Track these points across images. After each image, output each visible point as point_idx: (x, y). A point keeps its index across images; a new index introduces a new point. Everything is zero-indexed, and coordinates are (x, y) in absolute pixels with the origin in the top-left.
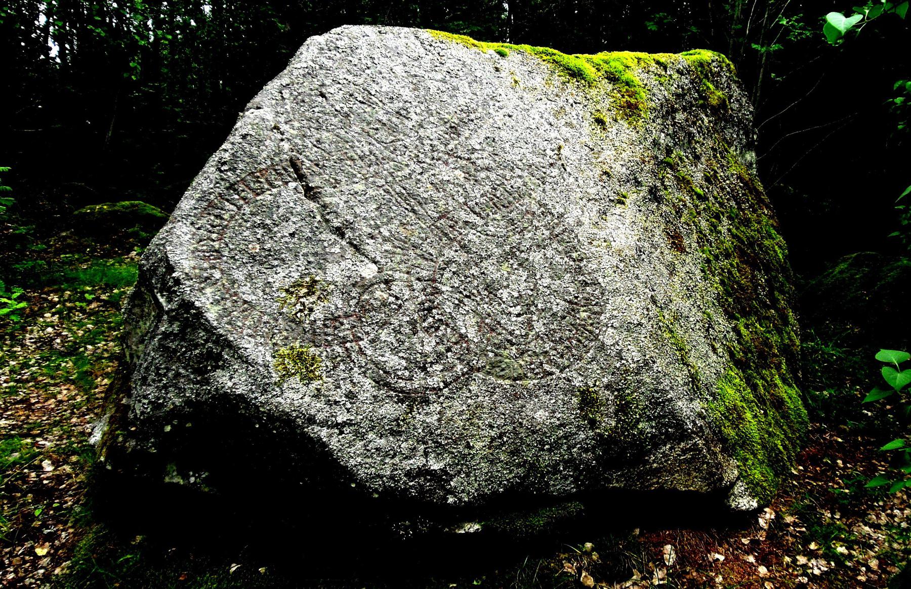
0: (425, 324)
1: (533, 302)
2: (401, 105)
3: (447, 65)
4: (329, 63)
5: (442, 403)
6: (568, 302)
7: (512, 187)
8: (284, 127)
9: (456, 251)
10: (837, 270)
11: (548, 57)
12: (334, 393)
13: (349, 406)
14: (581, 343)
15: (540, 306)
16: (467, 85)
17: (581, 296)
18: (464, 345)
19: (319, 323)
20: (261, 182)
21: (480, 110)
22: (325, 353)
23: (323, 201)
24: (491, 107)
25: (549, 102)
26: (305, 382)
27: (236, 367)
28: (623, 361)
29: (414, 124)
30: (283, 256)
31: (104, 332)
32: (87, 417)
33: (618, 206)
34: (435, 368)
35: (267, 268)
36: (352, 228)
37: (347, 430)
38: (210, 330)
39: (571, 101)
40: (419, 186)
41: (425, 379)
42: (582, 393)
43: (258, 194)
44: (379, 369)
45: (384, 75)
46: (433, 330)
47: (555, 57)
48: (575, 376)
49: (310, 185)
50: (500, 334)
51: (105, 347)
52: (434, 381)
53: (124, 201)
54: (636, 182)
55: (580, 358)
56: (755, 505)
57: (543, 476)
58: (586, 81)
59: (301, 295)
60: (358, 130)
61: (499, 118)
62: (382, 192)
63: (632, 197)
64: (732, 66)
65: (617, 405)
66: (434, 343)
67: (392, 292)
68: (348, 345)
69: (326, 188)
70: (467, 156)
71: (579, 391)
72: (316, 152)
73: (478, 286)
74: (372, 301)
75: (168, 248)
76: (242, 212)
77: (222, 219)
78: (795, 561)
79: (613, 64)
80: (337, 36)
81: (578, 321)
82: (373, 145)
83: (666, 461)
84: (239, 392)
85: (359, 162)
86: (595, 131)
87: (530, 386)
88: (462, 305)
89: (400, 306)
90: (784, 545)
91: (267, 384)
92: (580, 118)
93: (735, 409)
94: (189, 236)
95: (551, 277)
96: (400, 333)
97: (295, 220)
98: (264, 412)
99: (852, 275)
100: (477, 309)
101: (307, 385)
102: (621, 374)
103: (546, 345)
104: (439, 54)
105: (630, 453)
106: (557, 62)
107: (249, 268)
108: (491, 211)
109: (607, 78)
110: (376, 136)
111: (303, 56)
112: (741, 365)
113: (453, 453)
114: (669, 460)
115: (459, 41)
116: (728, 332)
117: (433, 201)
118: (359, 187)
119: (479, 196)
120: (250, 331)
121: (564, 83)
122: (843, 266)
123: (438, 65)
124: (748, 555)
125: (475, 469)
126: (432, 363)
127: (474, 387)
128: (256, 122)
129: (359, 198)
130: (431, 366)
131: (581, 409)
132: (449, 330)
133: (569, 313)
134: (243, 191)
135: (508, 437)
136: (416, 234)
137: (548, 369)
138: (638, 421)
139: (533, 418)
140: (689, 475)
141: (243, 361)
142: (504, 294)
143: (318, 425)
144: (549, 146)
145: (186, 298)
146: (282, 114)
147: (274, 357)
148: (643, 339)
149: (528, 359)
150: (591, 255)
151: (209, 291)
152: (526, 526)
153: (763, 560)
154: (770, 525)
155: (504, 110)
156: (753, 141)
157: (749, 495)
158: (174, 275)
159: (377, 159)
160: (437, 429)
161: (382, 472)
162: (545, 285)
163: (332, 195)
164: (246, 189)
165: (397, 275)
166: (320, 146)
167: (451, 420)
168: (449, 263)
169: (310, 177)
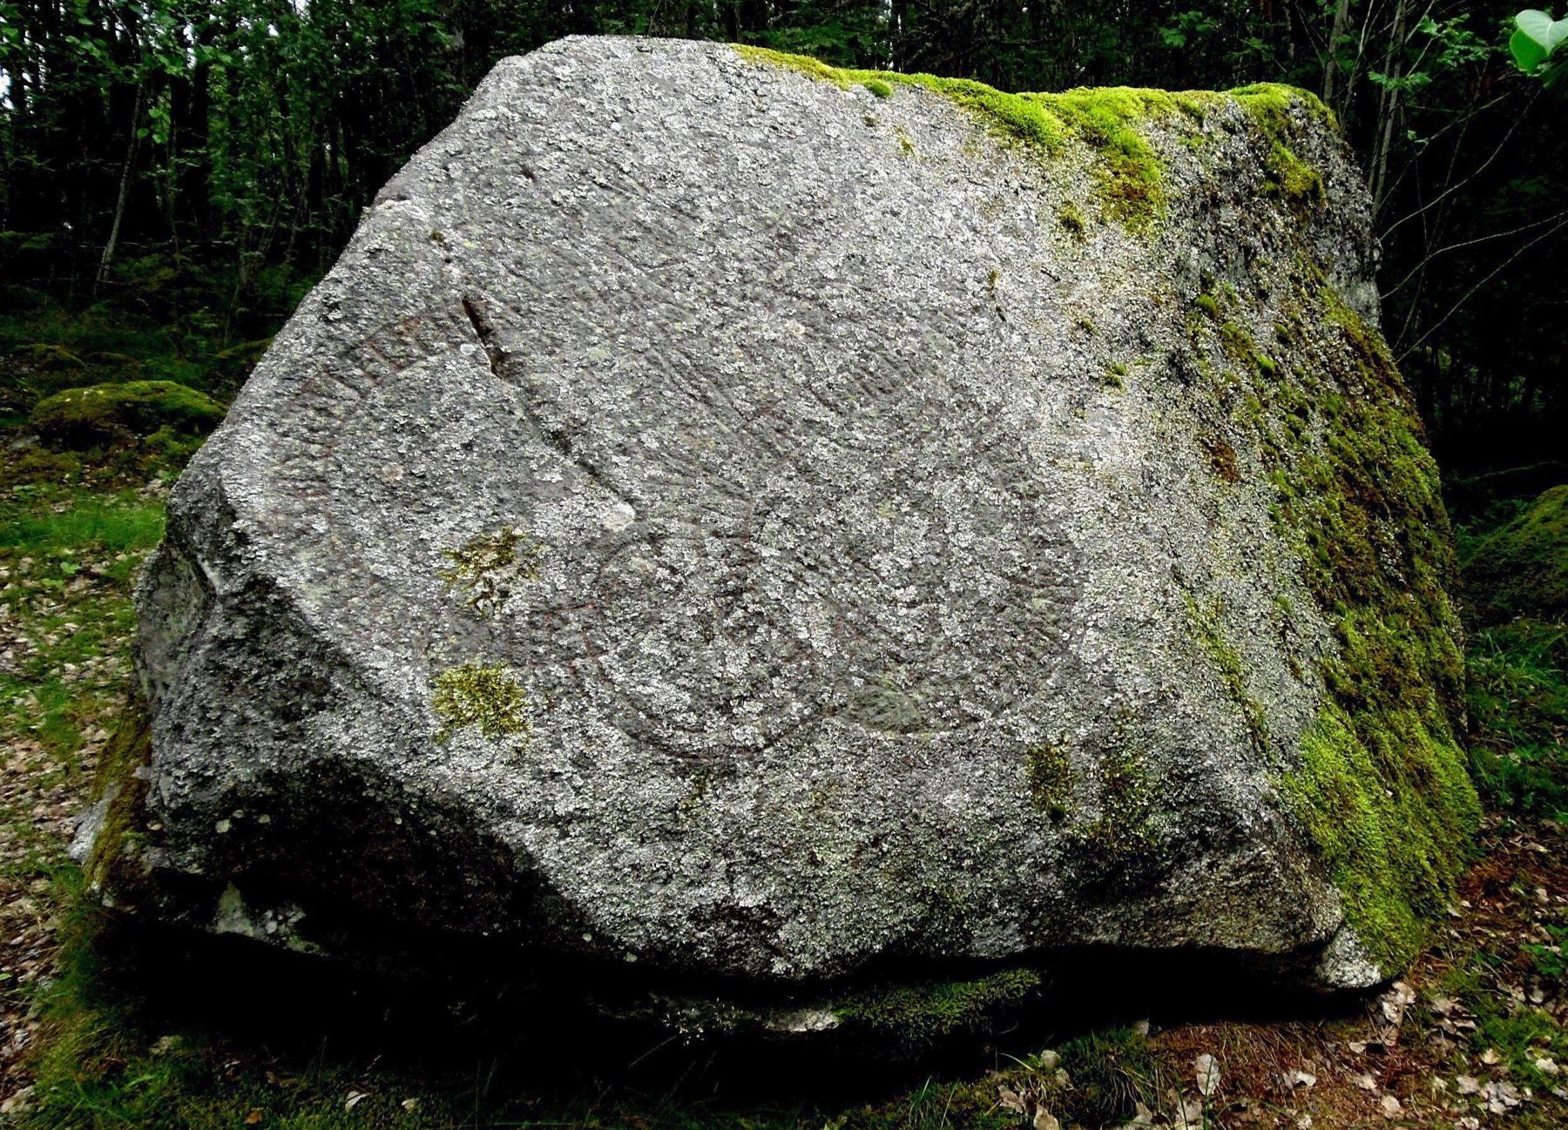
0: (729, 622)
2: (681, 191)
3: (773, 113)
5: (761, 777)
6: (1008, 578)
7: (898, 352)
8: (451, 236)
9: (790, 478)
11: (970, 98)
12: (550, 756)
13: (579, 782)
14: (1035, 658)
15: (953, 587)
17: (1035, 567)
18: (805, 663)
19: (521, 620)
20: (406, 344)
21: (836, 202)
22: (532, 680)
23: (529, 381)
24: (859, 196)
25: (972, 187)
27: (358, 706)
28: (1117, 695)
29: (706, 229)
30: (449, 488)
31: (97, 637)
35: (419, 513)
36: (584, 434)
37: (575, 829)
39: (1015, 184)
40: (715, 350)
41: (729, 729)
42: (1037, 756)
43: (401, 368)
44: (639, 710)
45: (649, 133)
46: (744, 633)
47: (983, 99)
50: (875, 641)
51: (101, 666)
52: (745, 734)
54: (1142, 342)
55: (1033, 689)
57: (960, 918)
58: (1043, 145)
60: (597, 240)
62: (645, 363)
63: (1135, 373)
66: (745, 660)
68: (578, 663)
70: (810, 292)
71: (1030, 753)
72: (514, 284)
75: (225, 473)
76: (370, 401)
77: (330, 415)
78: (1453, 1087)
79: (1097, 112)
80: (556, 57)
82: (627, 270)
83: (1200, 890)
84: (363, 754)
88: (801, 584)
89: (679, 587)
91: (420, 739)
94: (266, 449)
96: (680, 639)
97: (472, 417)
103: (966, 663)
104: (755, 91)
109: (1085, 139)
111: (488, 95)
113: (783, 874)
116: (1322, 637)
117: (744, 381)
118: (598, 353)
121: (1000, 149)
124: (1363, 1074)
125: (826, 907)
126: (742, 698)
127: (823, 746)
129: (598, 375)
130: (740, 705)
131: (1035, 788)
132: (775, 634)
133: (1010, 600)
134: (371, 360)
135: (892, 843)
136: (712, 444)
137: (969, 710)
138: (1146, 813)
139: (941, 805)
140: (1246, 916)
141: (371, 694)
142: (884, 563)
143: (519, 819)
145: (260, 570)
146: (448, 210)
147: (432, 686)
150: (1054, 486)
151: (304, 557)
153: (1391, 1083)
155: (884, 202)
157: (1364, 957)
158: (235, 526)
160: (752, 827)
161: (643, 913)
162: (964, 545)
163: (545, 369)
165: (674, 526)
166: (521, 272)
168: (775, 501)
169: (502, 334)
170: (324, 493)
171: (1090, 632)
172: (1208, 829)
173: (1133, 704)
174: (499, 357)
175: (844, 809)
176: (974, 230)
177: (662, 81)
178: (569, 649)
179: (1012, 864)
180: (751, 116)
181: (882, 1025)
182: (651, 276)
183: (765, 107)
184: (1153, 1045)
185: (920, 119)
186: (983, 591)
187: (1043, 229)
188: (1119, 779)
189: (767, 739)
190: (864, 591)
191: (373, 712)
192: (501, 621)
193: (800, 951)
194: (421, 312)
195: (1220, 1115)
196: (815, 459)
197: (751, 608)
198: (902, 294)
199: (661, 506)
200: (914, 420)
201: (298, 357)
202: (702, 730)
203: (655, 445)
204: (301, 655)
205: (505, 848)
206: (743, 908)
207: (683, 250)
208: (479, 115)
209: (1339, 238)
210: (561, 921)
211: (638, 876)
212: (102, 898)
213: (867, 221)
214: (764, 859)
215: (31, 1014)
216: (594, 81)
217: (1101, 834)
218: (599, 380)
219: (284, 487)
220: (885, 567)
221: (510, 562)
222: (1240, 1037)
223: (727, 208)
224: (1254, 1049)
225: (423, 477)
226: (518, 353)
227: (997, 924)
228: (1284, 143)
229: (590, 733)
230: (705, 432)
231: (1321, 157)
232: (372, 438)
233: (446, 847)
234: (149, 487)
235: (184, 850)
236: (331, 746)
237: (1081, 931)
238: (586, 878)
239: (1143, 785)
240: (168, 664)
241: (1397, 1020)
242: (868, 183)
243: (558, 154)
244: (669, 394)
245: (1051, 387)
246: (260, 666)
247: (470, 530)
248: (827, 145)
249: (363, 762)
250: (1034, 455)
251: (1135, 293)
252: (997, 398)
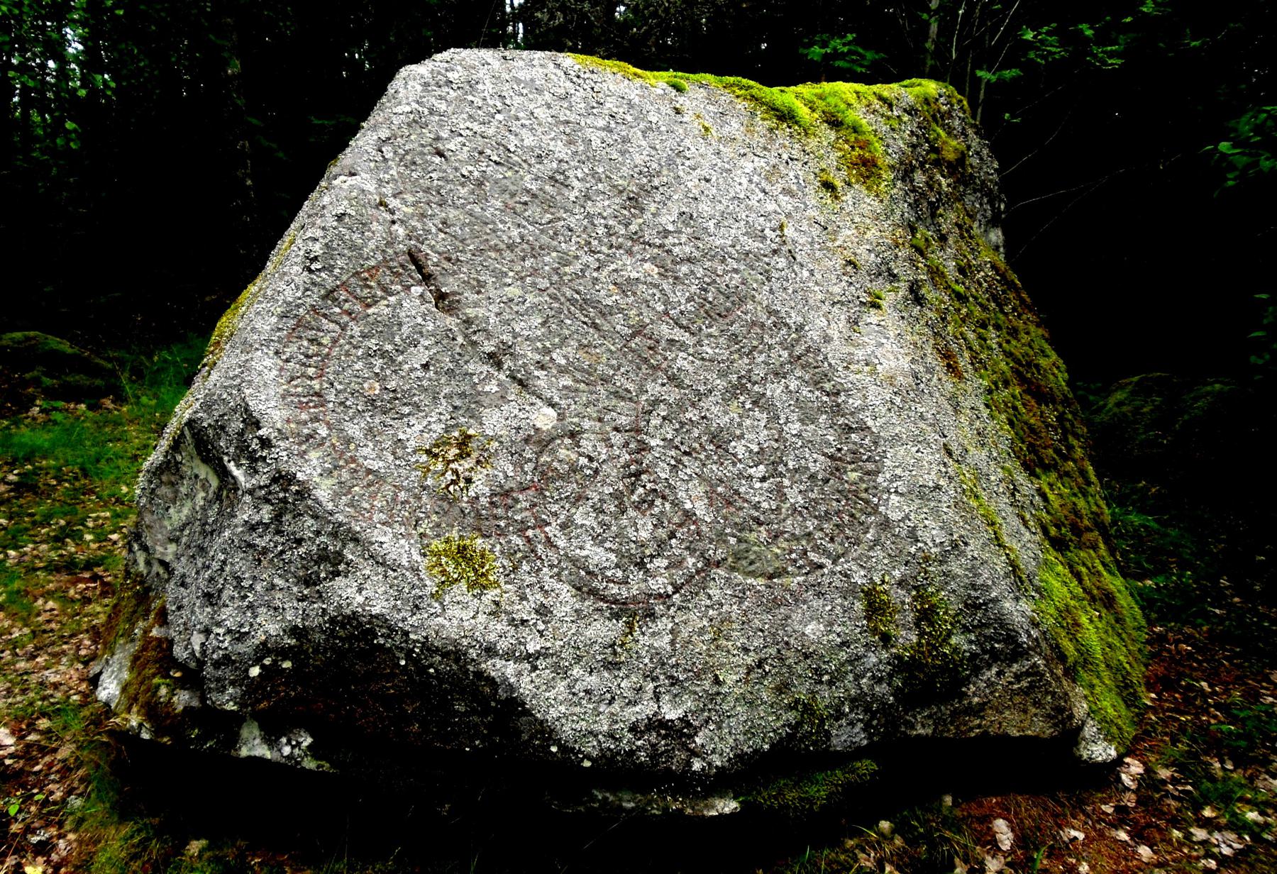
0: (635, 498)
1: (780, 458)
2: (555, 165)
3: (608, 105)
4: (443, 107)
5: (673, 617)
6: (829, 457)
7: (727, 285)
8: (394, 203)
9: (663, 385)
10: (1112, 401)
11: (743, 92)
12: (519, 607)
13: (541, 627)
14: (855, 518)
15: (791, 465)
16: (640, 134)
17: (846, 448)
18: (693, 527)
19: (484, 501)
20: (370, 287)
21: (665, 172)
22: (498, 547)
23: (465, 314)
24: (680, 167)
25: (756, 159)
26: (475, 592)
27: (367, 572)
28: (920, 545)
29: (577, 194)
30: (416, 399)
31: (27, 529)
32: (38, 659)
33: (873, 311)
34: (657, 564)
35: (394, 419)
36: (511, 354)
37: (541, 663)
39: (785, 156)
40: (597, 288)
41: (646, 581)
42: (868, 594)
43: (369, 306)
44: (579, 568)
45: (523, 121)
46: (646, 505)
47: (754, 92)
48: (854, 568)
49: (443, 290)
50: (741, 509)
51: (35, 552)
52: (659, 584)
53: (12, 331)
54: (890, 275)
55: (858, 542)
56: (1113, 753)
57: (822, 721)
58: (800, 126)
59: (451, 458)
60: (499, 204)
61: (692, 182)
62: (548, 299)
63: (888, 299)
64: (965, 103)
65: (917, 611)
66: (650, 527)
67: (582, 450)
68: (530, 533)
69: (466, 295)
70: (658, 242)
71: (863, 591)
72: (443, 240)
73: (699, 437)
74: (555, 464)
75: (247, 392)
76: (349, 333)
77: (320, 344)
78: (1188, 836)
79: (832, 100)
80: (446, 65)
81: (846, 485)
82: (524, 227)
83: (992, 693)
84: (376, 610)
85: (507, 254)
86: (824, 201)
87: (794, 586)
88: (681, 467)
89: (596, 472)
90: (1165, 813)
91: (420, 597)
92: (801, 182)
93: (1067, 611)
94: (275, 372)
95: (801, 420)
96: (603, 512)
97: (427, 343)
98: (418, 641)
99: (1137, 411)
100: (703, 472)
101: (478, 596)
102: (919, 564)
103: (809, 523)
104: (593, 88)
105: (940, 682)
106: (757, 100)
107: (368, 419)
108: (704, 324)
109: (826, 122)
110: (527, 214)
111: (400, 95)
112: (1059, 544)
113: (696, 693)
114: (996, 691)
115: (615, 70)
116: (1033, 496)
117: (621, 310)
118: (514, 291)
119: (683, 301)
120: (383, 516)
121: (771, 130)
122: (1120, 396)
123: (595, 105)
124: (1117, 829)
125: (728, 717)
126: (652, 556)
128: (354, 194)
129: (516, 309)
130: (651, 562)
131: (868, 618)
132: (668, 506)
133: (831, 474)
134: (346, 301)
135: (771, 665)
136: (604, 360)
137: (816, 560)
138: (950, 634)
139: (804, 634)
140: (1025, 711)
141: (377, 563)
142: (739, 448)
143: (501, 657)
144: (768, 225)
145: (284, 467)
146: (388, 183)
147: (424, 555)
148: (945, 510)
149: (785, 545)
150: (850, 386)
151: (313, 455)
152: (801, 799)
153: (1139, 835)
154: (1139, 784)
155: (698, 171)
156: (1000, 212)
157: (1105, 740)
158: (260, 433)
159: (533, 249)
160: (670, 657)
161: (595, 727)
162: (794, 432)
163: (476, 305)
164: (350, 298)
165: (587, 424)
166: (448, 230)
167: (688, 642)
168: (656, 402)
169: (440, 279)
171: (893, 496)
172: (996, 645)
173: (933, 550)
174: (440, 297)
175: (735, 640)
176: (764, 191)
177: (525, 82)
178: (522, 522)
179: (858, 677)
180: (593, 108)
181: (771, 807)
182: (542, 231)
183: (602, 101)
184: (958, 813)
185: (711, 108)
186: (813, 468)
187: (810, 190)
188: (928, 609)
189: (674, 587)
190: (729, 470)
192: (468, 502)
193: (712, 752)
194: (380, 262)
195: (1020, 863)
196: (679, 369)
197: (649, 486)
198: (722, 241)
199: (575, 409)
200: (745, 338)
201: (291, 300)
202: (627, 583)
203: (563, 362)
204: (318, 533)
205: (491, 681)
206: (668, 721)
207: (562, 211)
208: (399, 109)
209: (979, 195)
210: (532, 737)
211: (590, 699)
212: (140, 732)
213: (689, 186)
214: (682, 681)
215: (67, 827)
216: (477, 83)
217: (919, 652)
218: (517, 312)
219: (292, 401)
220: (741, 451)
221: (468, 455)
222: (1024, 804)
223: (589, 178)
224: (1034, 812)
225: (394, 391)
226: (454, 293)
227: (848, 724)
228: (937, 123)
229: (546, 588)
230: (598, 351)
231: (962, 133)
232: (353, 361)
233: (441, 681)
234: (30, 414)
235: (223, 692)
236: (348, 605)
237: (906, 728)
238: (553, 702)
239: (946, 613)
240: (169, 546)
241: (1133, 786)
242: (685, 157)
243: (461, 139)
244: (568, 322)
245: (835, 309)
246: (283, 544)
247: (435, 432)
248: (651, 129)
249: (376, 616)
250: (833, 362)
251: (882, 237)
252: (800, 319)
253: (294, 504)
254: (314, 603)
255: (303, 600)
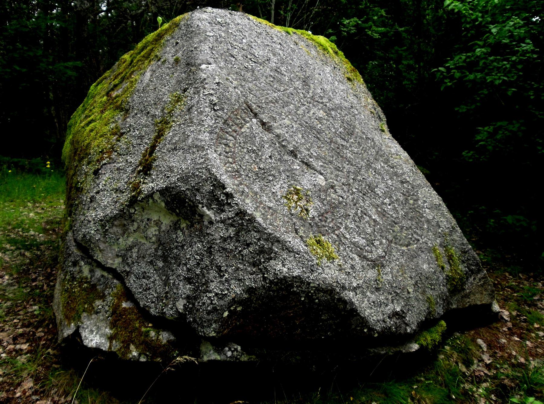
27: (285, 256)
38: (259, 230)
78: (537, 335)
83: (472, 287)
84: (295, 274)
91: (313, 265)
113: (403, 298)
134: (232, 125)
140: (482, 294)
141: (289, 251)
170: (240, 177)
191: (292, 258)
204: (259, 240)
205: (345, 302)
249: (296, 277)
253: (247, 226)
254: (258, 275)
255: (252, 274)
